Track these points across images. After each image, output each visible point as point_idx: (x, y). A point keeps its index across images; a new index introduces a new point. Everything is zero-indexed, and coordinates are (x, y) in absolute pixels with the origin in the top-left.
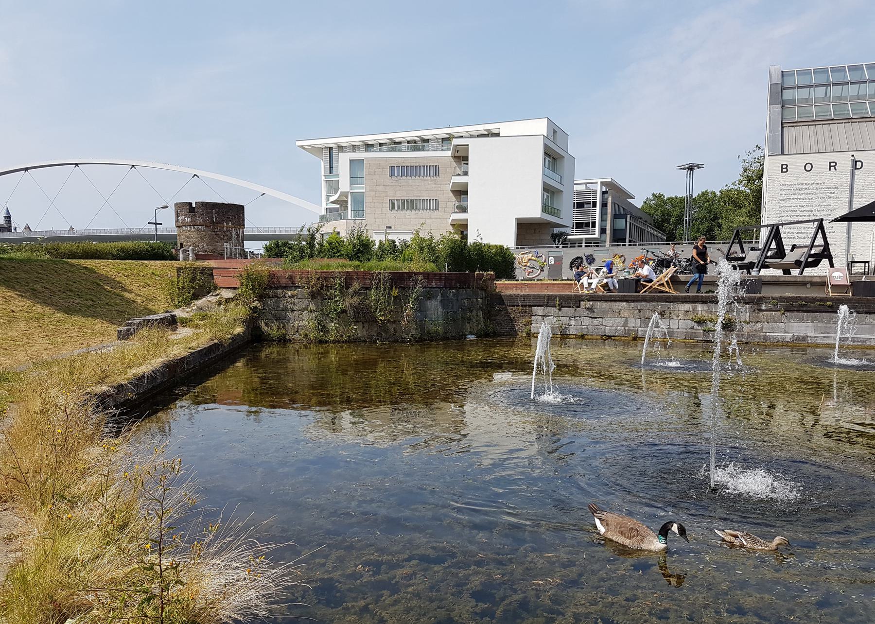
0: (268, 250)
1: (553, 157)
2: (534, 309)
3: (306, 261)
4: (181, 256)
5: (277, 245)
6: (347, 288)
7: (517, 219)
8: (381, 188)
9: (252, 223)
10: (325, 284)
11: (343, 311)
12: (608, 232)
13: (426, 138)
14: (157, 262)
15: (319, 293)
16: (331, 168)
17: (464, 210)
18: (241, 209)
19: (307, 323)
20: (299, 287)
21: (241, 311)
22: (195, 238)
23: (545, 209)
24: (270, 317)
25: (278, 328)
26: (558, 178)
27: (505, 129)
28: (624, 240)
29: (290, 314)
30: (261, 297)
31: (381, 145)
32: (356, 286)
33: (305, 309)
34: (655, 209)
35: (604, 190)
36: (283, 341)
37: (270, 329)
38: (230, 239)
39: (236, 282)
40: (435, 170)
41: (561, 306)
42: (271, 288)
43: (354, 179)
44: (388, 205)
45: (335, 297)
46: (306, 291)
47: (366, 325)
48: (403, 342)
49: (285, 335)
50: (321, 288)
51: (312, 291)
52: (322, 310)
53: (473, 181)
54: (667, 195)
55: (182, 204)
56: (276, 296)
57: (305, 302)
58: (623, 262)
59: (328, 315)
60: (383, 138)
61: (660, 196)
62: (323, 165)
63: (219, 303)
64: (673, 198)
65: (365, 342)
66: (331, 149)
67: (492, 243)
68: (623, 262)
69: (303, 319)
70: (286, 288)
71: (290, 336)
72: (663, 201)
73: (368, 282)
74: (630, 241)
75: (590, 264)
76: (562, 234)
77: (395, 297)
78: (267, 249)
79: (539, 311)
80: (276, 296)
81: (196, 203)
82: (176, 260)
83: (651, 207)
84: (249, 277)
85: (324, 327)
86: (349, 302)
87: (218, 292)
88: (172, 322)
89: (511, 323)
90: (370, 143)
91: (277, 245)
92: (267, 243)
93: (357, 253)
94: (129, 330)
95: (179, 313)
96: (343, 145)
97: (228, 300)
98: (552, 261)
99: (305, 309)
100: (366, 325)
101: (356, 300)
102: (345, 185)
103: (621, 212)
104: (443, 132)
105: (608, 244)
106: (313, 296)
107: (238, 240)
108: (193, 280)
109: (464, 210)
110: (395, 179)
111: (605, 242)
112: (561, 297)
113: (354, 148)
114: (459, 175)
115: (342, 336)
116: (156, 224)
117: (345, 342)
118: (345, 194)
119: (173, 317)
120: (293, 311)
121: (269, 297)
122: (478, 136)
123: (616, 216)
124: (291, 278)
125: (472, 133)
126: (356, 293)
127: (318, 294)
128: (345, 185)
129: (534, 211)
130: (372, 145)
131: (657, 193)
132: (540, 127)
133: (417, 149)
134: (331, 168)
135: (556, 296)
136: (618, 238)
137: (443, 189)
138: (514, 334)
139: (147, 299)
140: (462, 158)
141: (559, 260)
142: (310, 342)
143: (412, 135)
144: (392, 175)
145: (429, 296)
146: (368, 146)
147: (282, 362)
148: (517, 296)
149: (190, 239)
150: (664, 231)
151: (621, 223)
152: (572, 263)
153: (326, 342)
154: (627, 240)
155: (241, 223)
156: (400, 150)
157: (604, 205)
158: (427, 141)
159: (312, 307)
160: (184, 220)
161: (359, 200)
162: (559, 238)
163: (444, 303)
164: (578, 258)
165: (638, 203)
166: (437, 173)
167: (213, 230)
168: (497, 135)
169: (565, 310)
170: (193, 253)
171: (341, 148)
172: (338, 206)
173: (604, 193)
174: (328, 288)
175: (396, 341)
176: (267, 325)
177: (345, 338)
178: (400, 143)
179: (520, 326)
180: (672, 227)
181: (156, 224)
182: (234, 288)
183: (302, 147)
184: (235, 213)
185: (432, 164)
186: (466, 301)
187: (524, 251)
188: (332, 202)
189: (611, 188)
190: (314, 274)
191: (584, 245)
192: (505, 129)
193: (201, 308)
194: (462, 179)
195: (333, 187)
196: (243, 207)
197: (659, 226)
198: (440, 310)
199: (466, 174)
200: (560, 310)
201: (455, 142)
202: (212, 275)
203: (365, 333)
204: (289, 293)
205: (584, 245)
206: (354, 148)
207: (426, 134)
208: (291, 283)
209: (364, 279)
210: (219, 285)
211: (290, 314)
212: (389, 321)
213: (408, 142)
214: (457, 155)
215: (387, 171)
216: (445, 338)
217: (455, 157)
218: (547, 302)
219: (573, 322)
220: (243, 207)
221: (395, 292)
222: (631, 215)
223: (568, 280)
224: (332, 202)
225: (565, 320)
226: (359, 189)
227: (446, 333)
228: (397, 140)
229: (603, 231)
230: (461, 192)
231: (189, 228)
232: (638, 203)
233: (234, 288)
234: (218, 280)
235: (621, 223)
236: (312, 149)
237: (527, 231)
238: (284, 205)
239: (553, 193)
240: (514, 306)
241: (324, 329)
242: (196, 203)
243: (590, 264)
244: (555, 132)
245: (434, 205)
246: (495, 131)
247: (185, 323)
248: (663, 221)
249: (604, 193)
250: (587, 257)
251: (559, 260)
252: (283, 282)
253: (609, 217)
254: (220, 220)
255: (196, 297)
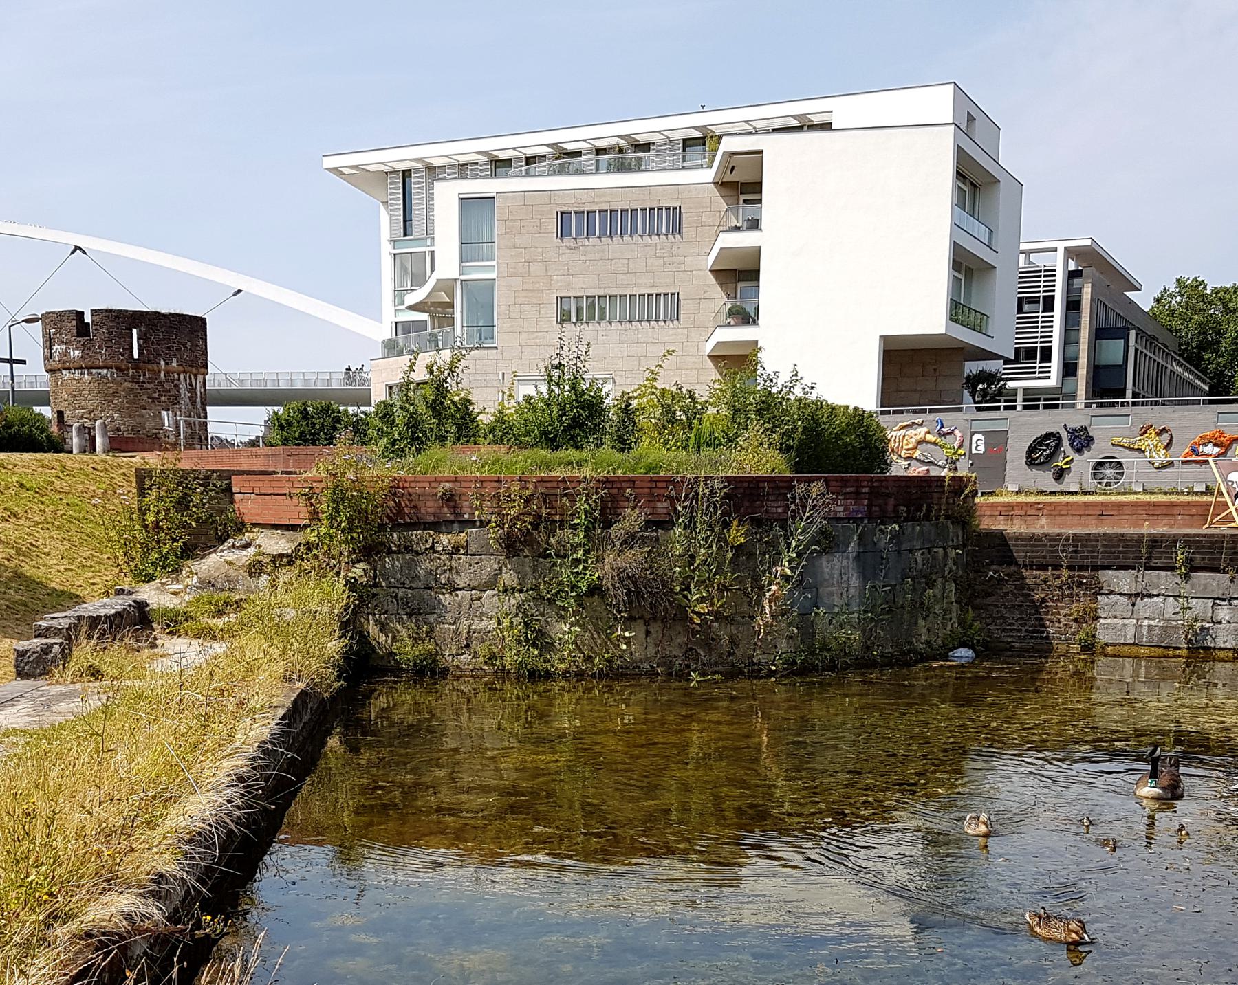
0: (282, 427)
1: (975, 183)
2: (1107, 576)
3: (434, 452)
4: (75, 441)
5: (305, 414)
6: (608, 525)
7: (885, 340)
8: (536, 268)
9: (227, 361)
10: (544, 512)
11: (596, 590)
12: (1082, 372)
13: (643, 139)
14: (26, 456)
15: (529, 540)
16: (406, 221)
17: (746, 317)
18: (197, 326)
19: (493, 624)
20: (472, 523)
21: (328, 595)
22: (92, 399)
23: (958, 311)
24: (392, 607)
25: (417, 639)
26: (983, 233)
27: (843, 111)
28: (1122, 393)
29: (446, 598)
30: (369, 551)
31: (530, 160)
32: (631, 518)
33: (491, 583)
34: (1184, 317)
35: (1072, 266)
36: (429, 672)
37: (400, 641)
38: (175, 400)
39: (298, 511)
40: (670, 219)
41: (1193, 568)
42: (396, 526)
43: (469, 246)
44: (553, 311)
45: (574, 548)
46: (492, 535)
47: (655, 628)
48: (755, 675)
49: (433, 657)
50: (536, 526)
51: (509, 535)
52: (535, 588)
53: (778, 238)
54: (1214, 282)
55: (60, 315)
56: (408, 549)
57: (490, 565)
58: (1167, 447)
59: (551, 602)
60: (536, 143)
61: (1198, 285)
62: (386, 221)
63: (255, 569)
64: (1226, 291)
65: (653, 674)
66: (406, 174)
67: (831, 401)
68: (1167, 447)
69: (480, 611)
70: (437, 525)
71: (449, 657)
72: (1203, 298)
73: (662, 506)
74: (1135, 395)
75: (1079, 451)
76: (989, 378)
77: (738, 549)
78: (279, 424)
79: (1123, 580)
80: (408, 549)
81: (94, 312)
82: (58, 450)
83: (1173, 313)
84: (338, 498)
85: (541, 633)
86: (613, 563)
87: (247, 537)
88: (138, 621)
89: (1035, 615)
90: (502, 155)
91: (305, 414)
92: (280, 410)
93: (570, 427)
94: (47, 650)
95: (154, 595)
96: (436, 162)
97: (277, 559)
98: (979, 444)
99: (491, 583)
100: (655, 628)
101: (633, 559)
102: (447, 265)
103: (1111, 323)
104: (686, 124)
105: (1081, 402)
106: (511, 547)
107: (194, 403)
108: (183, 504)
109: (746, 317)
110: (572, 243)
111: (1074, 398)
112: (1190, 541)
113: (464, 170)
114: (737, 228)
115: (588, 659)
116: (11, 361)
117: (600, 676)
118: (446, 286)
119: (141, 606)
120: (454, 589)
121: (390, 552)
122: (774, 130)
123: (1100, 334)
124: (450, 498)
125: (757, 125)
126: (630, 540)
127: (526, 543)
128: (447, 265)
129: (928, 317)
130: (508, 162)
131: (1189, 276)
132: (938, 104)
133: (624, 167)
134: (406, 221)
135: (1174, 539)
136: (1106, 386)
137: (692, 264)
138: (1045, 649)
139: (18, 551)
140: (743, 186)
141: (997, 441)
142: (502, 674)
143: (609, 134)
144: (563, 233)
145: (827, 542)
146: (500, 165)
147: (420, 733)
148: (1055, 539)
149: (75, 399)
150: (1204, 371)
151: (1113, 351)
152: (1032, 450)
153: (548, 676)
154: (1129, 393)
155: (198, 361)
156: (579, 172)
157: (1073, 305)
158: (646, 147)
159: (508, 578)
160: (65, 354)
161: (481, 298)
162: (989, 392)
163: (867, 564)
164: (1048, 436)
165: (1144, 300)
166: (676, 228)
167: (135, 380)
168: (827, 126)
169: (1201, 578)
170: (104, 434)
171: (432, 171)
172: (424, 316)
173: (1072, 275)
174: (552, 526)
175: (734, 673)
176: (383, 628)
177: (598, 664)
178: (578, 154)
179: (1061, 623)
180: (1223, 361)
181: (11, 361)
182: (293, 528)
183: (336, 171)
184: (181, 336)
185: (664, 204)
186: (918, 555)
187: (908, 419)
188: (412, 308)
189: (1089, 261)
190: (515, 487)
191: (1019, 404)
192: (843, 111)
193: (208, 583)
194: (745, 239)
195: (412, 269)
196: (202, 321)
197: (1193, 359)
198: (855, 581)
199: (754, 225)
200: (1186, 577)
201: (728, 145)
202: (228, 490)
203: (651, 650)
204: (445, 539)
205: (1019, 404)
206: (464, 170)
207: (641, 129)
208: (451, 513)
209: (652, 498)
210: (248, 519)
211: (446, 598)
212: (718, 616)
213: (599, 151)
214: (729, 178)
215: (552, 225)
216: (864, 664)
217: (722, 185)
218: (1149, 554)
219: (1224, 613)
220: (202, 321)
221: (737, 534)
222: (1140, 332)
223: (1145, 492)
224: (412, 308)
225: (1201, 607)
226: (481, 272)
227: (867, 648)
228: (570, 147)
229: (1069, 370)
230: (741, 274)
231: (77, 374)
232: (1144, 300)
233: (293, 528)
234: (247, 505)
235: (1113, 351)
236: (361, 177)
237: (912, 368)
238: (302, 320)
239: (970, 273)
240: (1045, 568)
241: (541, 640)
242: (94, 312)
243: (1079, 451)
244: (971, 119)
245: (669, 307)
246: (817, 119)
247: (175, 623)
248: (1202, 347)
249: (1072, 275)
250: (1073, 433)
251: (997, 441)
252: (429, 508)
253: (1084, 335)
254: (151, 353)
255: (190, 551)
